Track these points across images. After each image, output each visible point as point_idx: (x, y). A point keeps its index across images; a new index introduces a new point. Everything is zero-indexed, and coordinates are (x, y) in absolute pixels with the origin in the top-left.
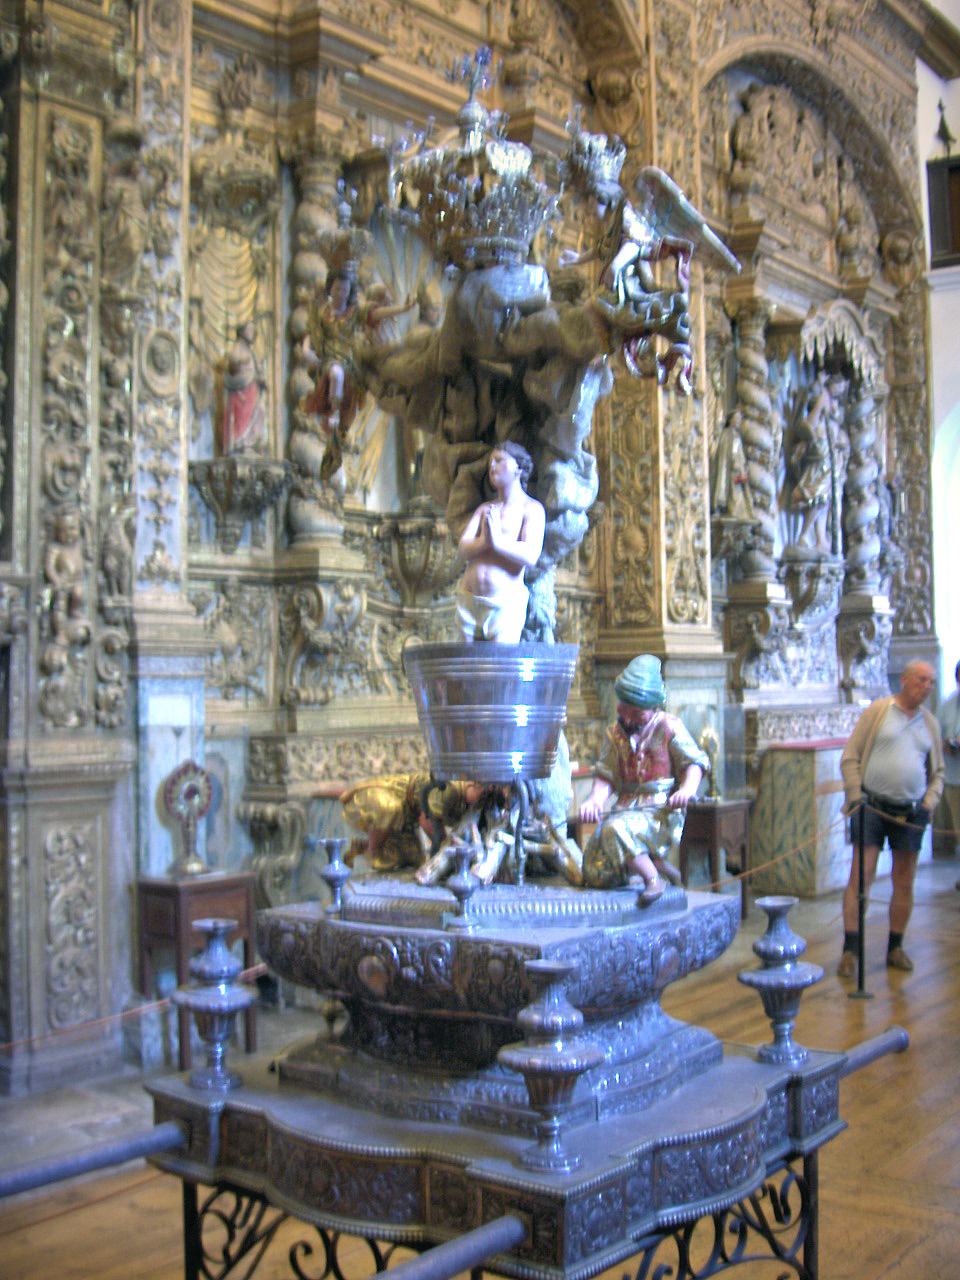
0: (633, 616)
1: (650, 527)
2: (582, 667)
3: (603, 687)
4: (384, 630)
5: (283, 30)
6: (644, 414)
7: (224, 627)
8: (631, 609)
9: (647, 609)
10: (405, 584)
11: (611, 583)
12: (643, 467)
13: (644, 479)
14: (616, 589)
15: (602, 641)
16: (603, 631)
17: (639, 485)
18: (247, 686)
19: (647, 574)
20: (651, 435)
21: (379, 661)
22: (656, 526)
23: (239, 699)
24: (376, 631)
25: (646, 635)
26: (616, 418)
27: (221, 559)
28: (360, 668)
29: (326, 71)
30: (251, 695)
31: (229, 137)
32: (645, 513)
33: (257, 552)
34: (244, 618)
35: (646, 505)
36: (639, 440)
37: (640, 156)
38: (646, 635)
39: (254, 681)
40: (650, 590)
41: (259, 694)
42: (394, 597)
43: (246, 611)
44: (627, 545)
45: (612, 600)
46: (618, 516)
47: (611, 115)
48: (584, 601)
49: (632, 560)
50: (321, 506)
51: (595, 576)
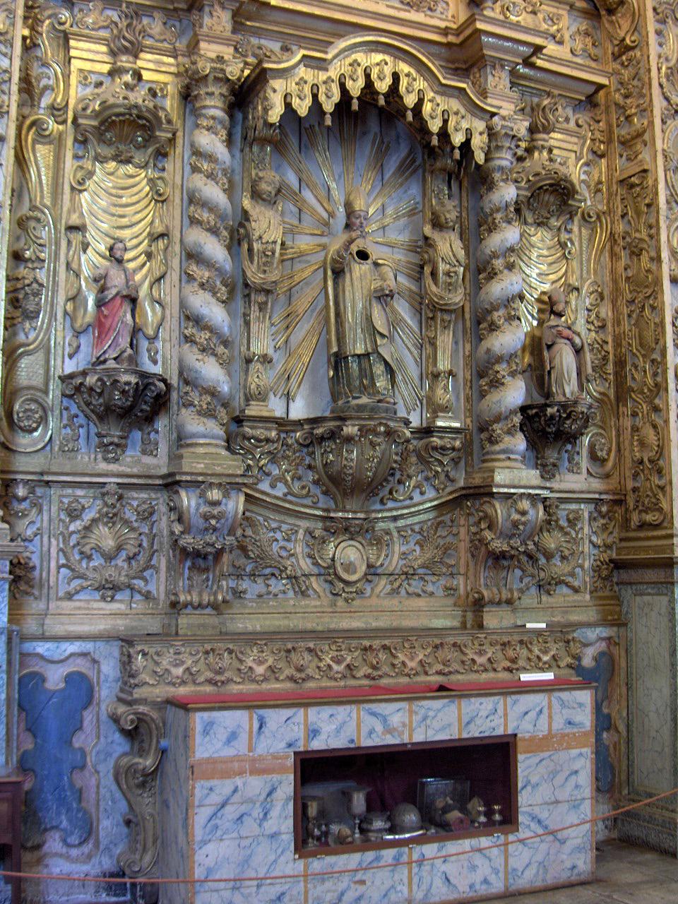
0: (649, 518)
1: (660, 422)
2: (596, 570)
3: (623, 592)
4: (309, 532)
5: (451, 39)
6: (653, 308)
7: (103, 530)
8: (646, 510)
9: (661, 510)
10: (333, 489)
11: (630, 484)
12: (653, 361)
13: (655, 375)
14: (635, 490)
15: (624, 544)
16: (624, 535)
17: (650, 381)
18: (132, 588)
19: (660, 472)
20: (659, 329)
21: (305, 565)
22: (667, 422)
23: (121, 601)
24: (301, 535)
25: (654, 538)
26: (629, 316)
27: (103, 466)
28: (279, 572)
29: (494, 67)
30: (138, 597)
31: (536, 154)
32: (656, 409)
33: (148, 460)
34: (562, 528)
35: (657, 401)
36: (649, 335)
37: (638, 54)
38: (654, 538)
39: (139, 583)
40: (662, 488)
41: (147, 596)
42: (324, 501)
43: (563, 523)
44: (642, 444)
45: (631, 502)
46: (635, 415)
47: (612, 22)
48: (597, 502)
49: (646, 460)
50: (199, 413)
51: (616, 477)
